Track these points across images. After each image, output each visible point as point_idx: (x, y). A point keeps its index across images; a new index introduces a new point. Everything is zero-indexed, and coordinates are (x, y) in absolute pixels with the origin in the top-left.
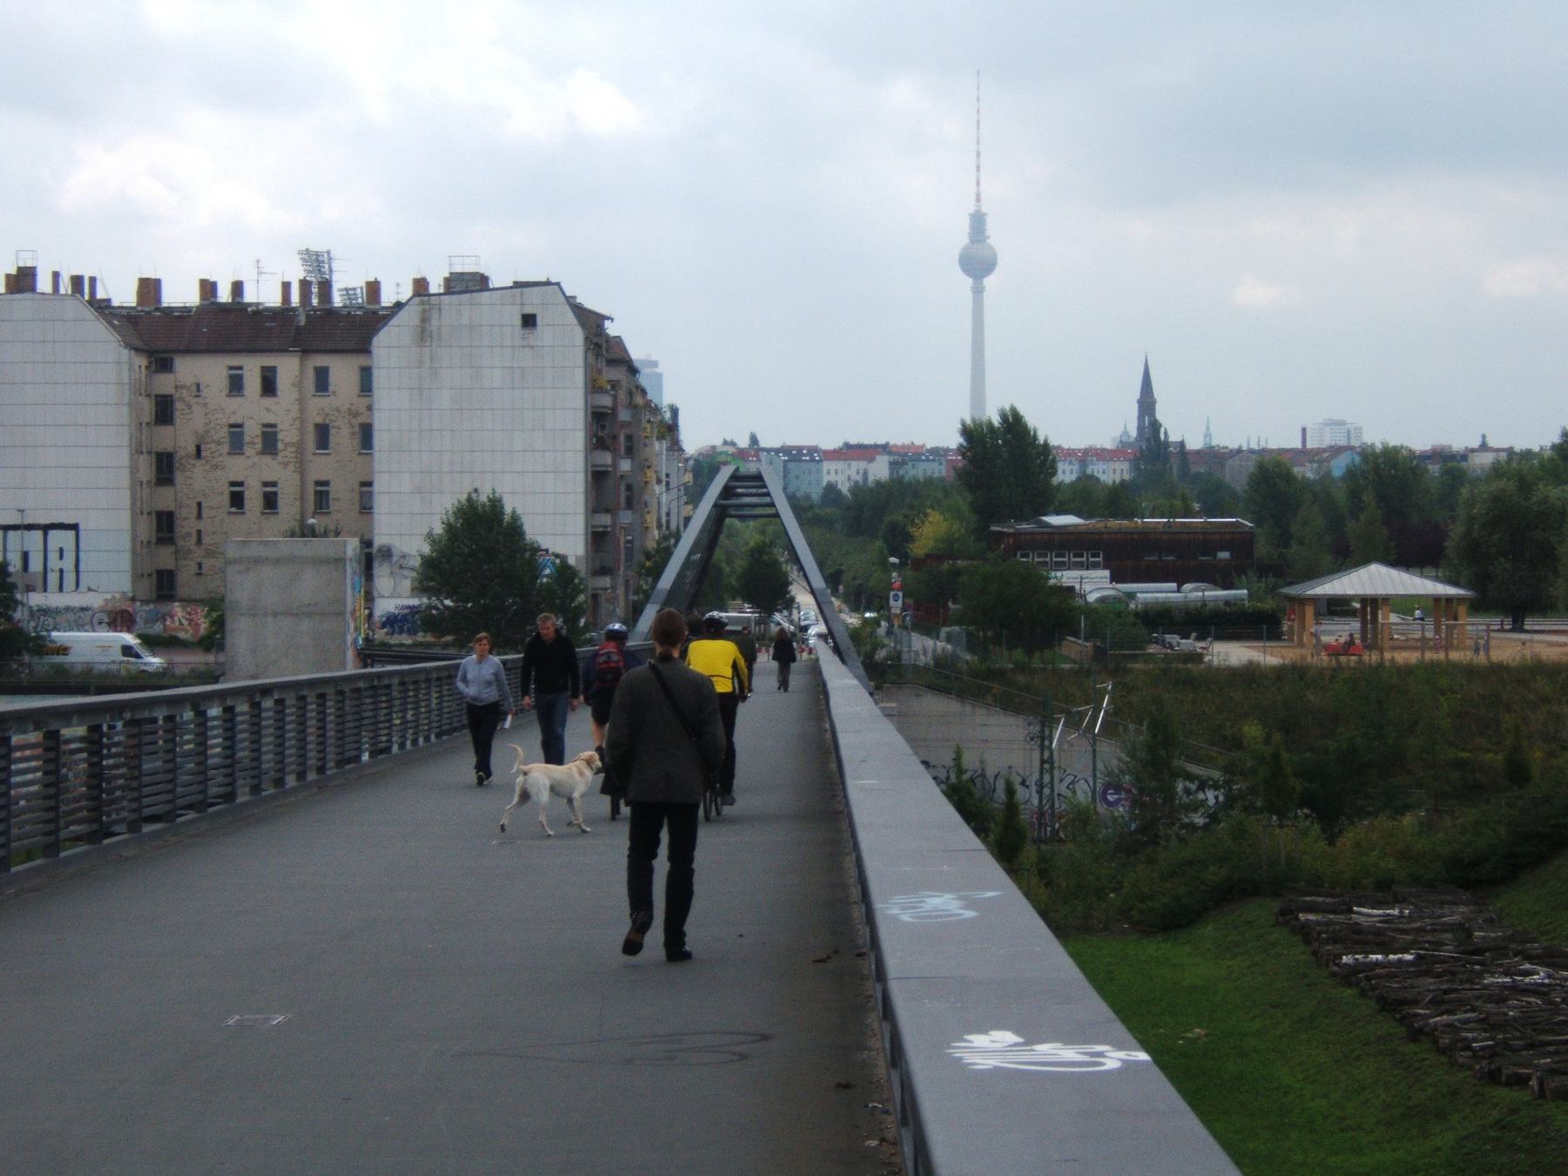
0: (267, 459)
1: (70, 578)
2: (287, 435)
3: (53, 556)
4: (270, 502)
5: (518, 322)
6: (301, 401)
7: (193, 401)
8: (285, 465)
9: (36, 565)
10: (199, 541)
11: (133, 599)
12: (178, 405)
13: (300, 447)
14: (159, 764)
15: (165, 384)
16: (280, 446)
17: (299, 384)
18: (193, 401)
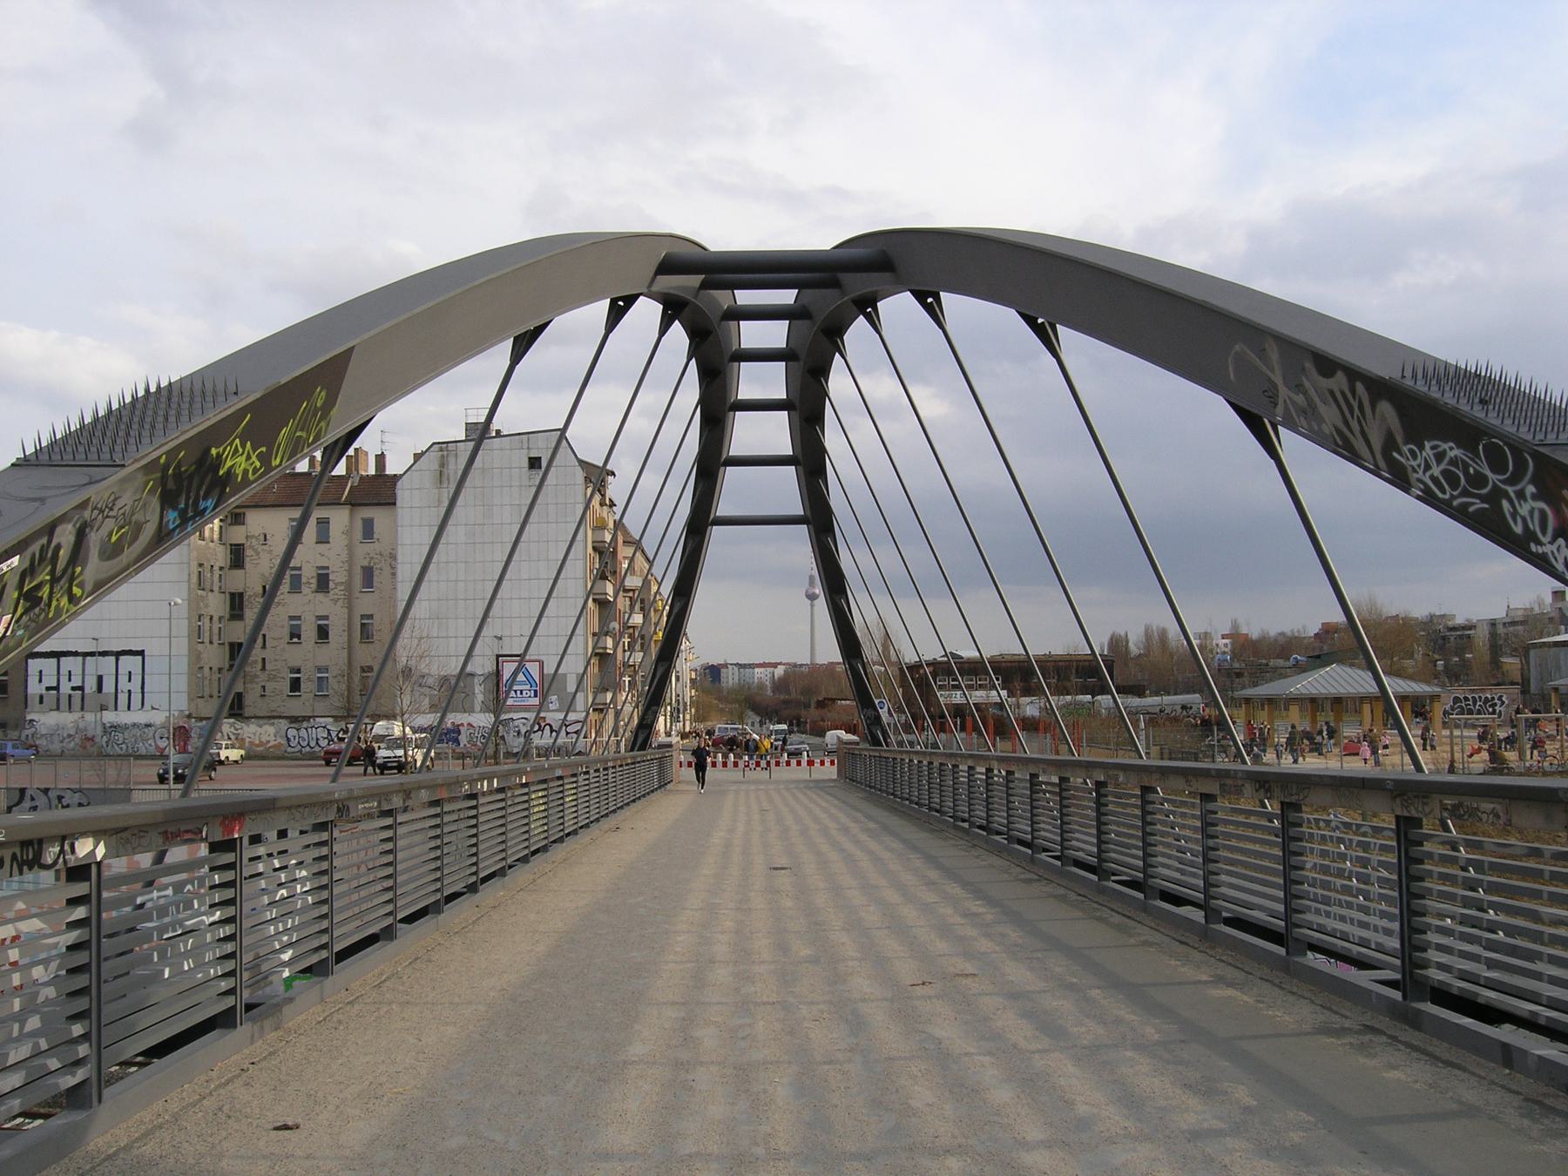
0: (320, 596)
1: (136, 698)
2: (338, 576)
3: (123, 679)
4: (323, 633)
5: (526, 463)
6: (350, 548)
7: (260, 548)
8: (335, 601)
9: (108, 687)
10: (264, 668)
11: (189, 716)
12: (248, 552)
13: (349, 586)
14: (203, 850)
15: (238, 534)
16: (331, 585)
17: (349, 532)
18: (260, 548)
